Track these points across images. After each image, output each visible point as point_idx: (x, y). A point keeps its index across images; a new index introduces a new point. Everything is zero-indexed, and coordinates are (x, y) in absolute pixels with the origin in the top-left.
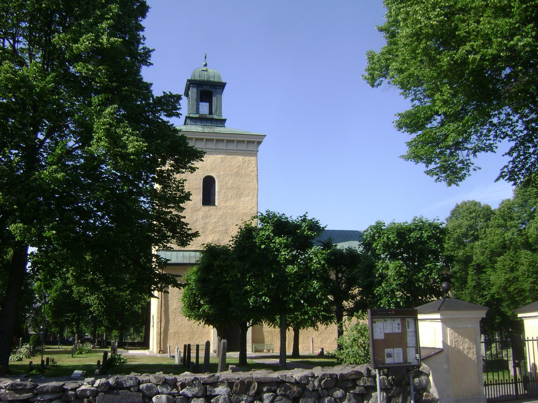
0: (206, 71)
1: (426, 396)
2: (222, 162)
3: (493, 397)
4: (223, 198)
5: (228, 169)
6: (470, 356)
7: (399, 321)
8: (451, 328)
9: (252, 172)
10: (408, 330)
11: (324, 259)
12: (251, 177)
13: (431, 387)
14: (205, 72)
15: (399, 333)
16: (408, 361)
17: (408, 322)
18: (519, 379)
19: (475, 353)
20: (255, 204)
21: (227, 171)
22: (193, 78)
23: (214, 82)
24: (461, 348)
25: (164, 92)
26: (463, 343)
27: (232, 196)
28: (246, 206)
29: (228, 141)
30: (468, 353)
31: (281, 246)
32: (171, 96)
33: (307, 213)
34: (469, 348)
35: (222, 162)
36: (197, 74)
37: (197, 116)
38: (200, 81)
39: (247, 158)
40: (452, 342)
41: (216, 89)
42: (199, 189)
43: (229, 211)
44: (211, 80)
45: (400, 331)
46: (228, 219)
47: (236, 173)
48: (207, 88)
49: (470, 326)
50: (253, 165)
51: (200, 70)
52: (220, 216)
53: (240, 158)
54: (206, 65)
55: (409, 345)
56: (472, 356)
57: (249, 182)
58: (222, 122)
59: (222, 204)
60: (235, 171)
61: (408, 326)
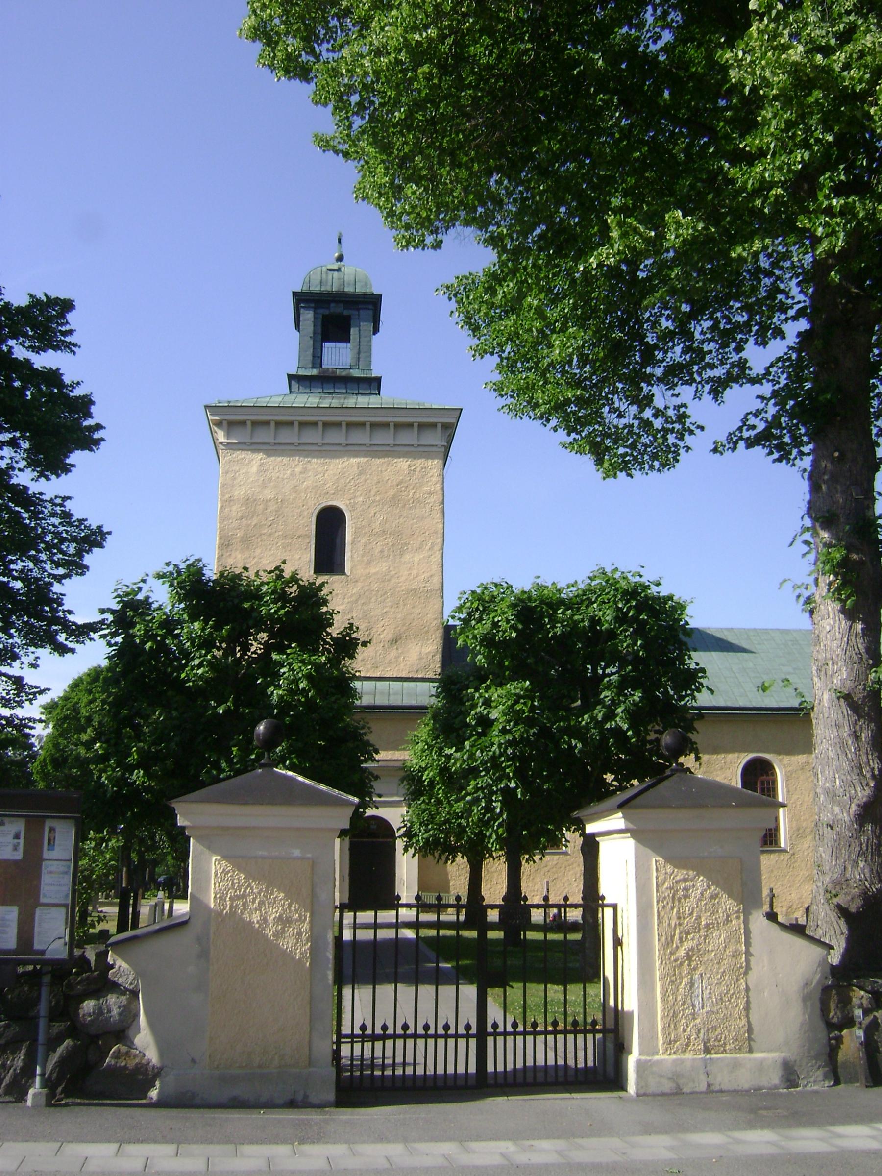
0: (339, 270)
1: (118, 1055)
2: (360, 474)
3: (500, 1068)
4: (363, 556)
5: (374, 490)
6: (287, 943)
7: (19, 826)
8: (225, 857)
9: (430, 493)
10: (46, 854)
11: (308, 677)
12: (428, 507)
13: (139, 1031)
14: (336, 273)
15: (16, 862)
16: (37, 946)
17: (52, 830)
18: (495, 1026)
19: (304, 937)
20: (435, 568)
21: (373, 493)
22: (305, 289)
23: (354, 295)
24: (256, 917)
25: (31, 296)
26: (262, 903)
27: (382, 551)
28: (414, 572)
29: (374, 426)
30: (277, 935)
31: (193, 644)
32: (52, 302)
33: (284, 562)
34: (284, 921)
35: (360, 474)
36: (316, 279)
37: (315, 372)
38: (321, 294)
39: (419, 463)
40: (222, 898)
41: (358, 310)
42: (309, 537)
43: (375, 586)
44: (346, 290)
45: (19, 855)
46: (372, 605)
47: (394, 497)
48: (336, 309)
49: (297, 853)
50: (434, 479)
51: (324, 269)
52: (354, 598)
53: (403, 464)
54: (340, 258)
55: (43, 900)
56: (295, 943)
57: (422, 518)
58: (374, 384)
59: (360, 571)
60: (391, 493)
61: (51, 843)
